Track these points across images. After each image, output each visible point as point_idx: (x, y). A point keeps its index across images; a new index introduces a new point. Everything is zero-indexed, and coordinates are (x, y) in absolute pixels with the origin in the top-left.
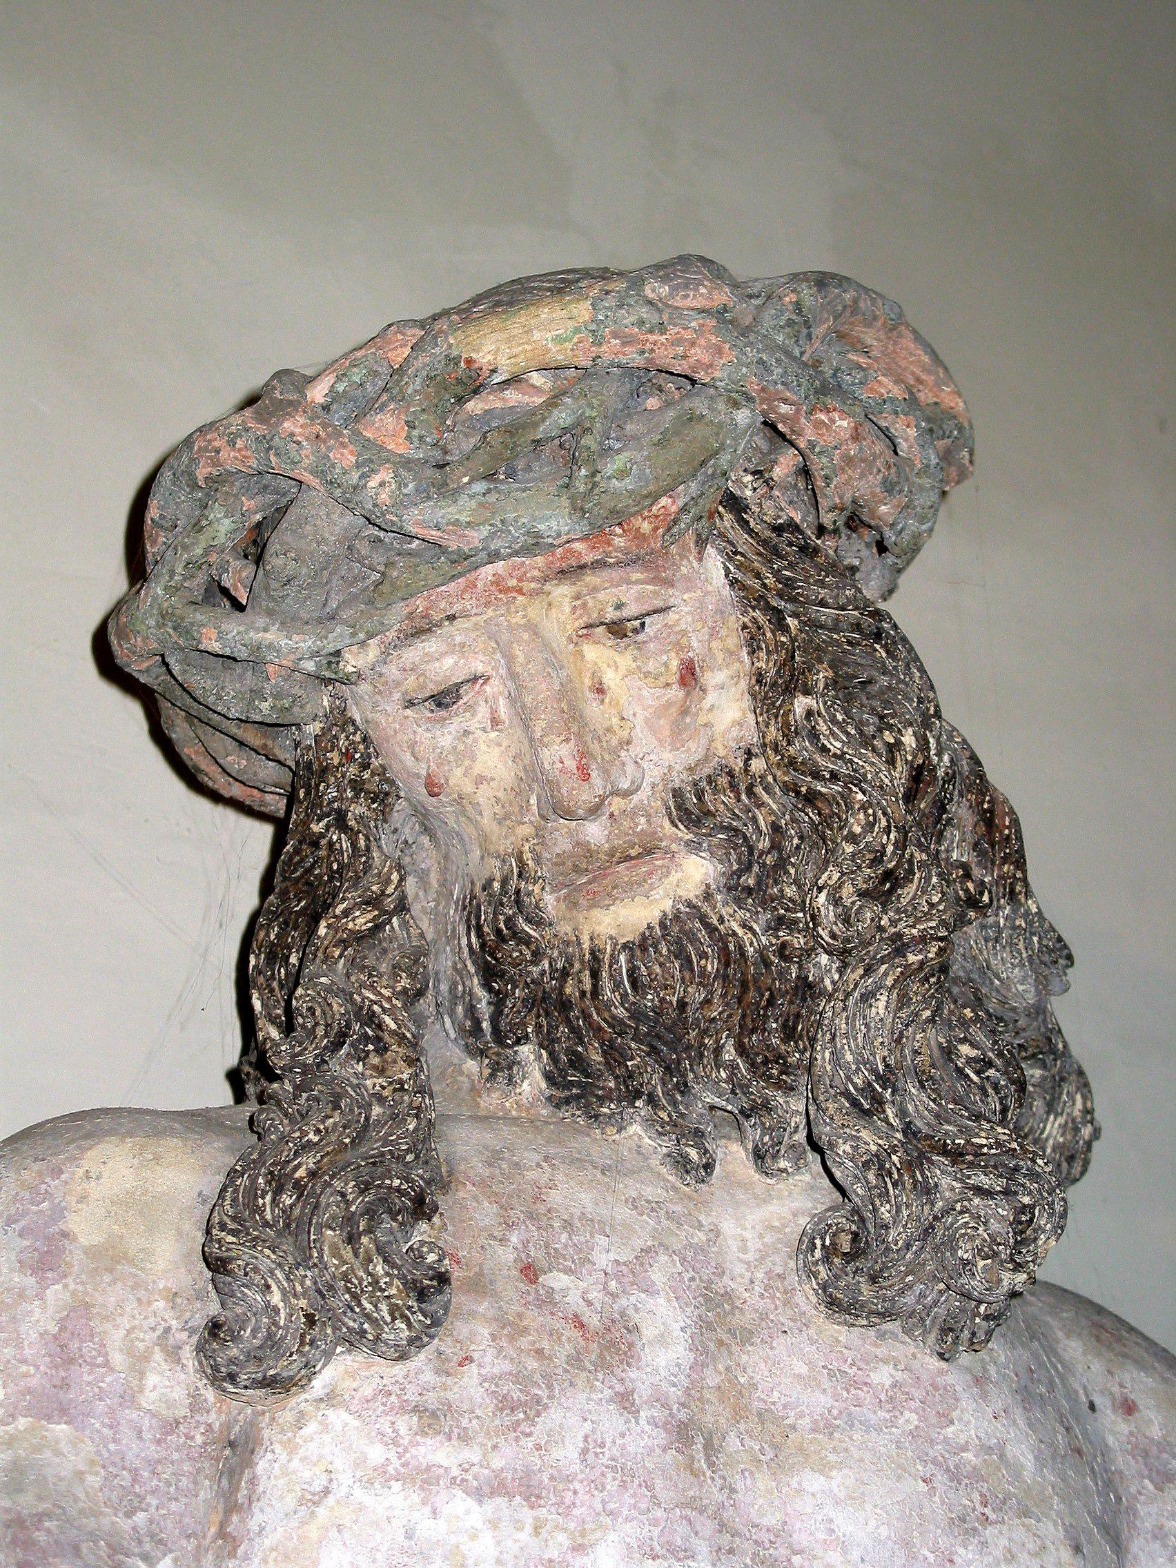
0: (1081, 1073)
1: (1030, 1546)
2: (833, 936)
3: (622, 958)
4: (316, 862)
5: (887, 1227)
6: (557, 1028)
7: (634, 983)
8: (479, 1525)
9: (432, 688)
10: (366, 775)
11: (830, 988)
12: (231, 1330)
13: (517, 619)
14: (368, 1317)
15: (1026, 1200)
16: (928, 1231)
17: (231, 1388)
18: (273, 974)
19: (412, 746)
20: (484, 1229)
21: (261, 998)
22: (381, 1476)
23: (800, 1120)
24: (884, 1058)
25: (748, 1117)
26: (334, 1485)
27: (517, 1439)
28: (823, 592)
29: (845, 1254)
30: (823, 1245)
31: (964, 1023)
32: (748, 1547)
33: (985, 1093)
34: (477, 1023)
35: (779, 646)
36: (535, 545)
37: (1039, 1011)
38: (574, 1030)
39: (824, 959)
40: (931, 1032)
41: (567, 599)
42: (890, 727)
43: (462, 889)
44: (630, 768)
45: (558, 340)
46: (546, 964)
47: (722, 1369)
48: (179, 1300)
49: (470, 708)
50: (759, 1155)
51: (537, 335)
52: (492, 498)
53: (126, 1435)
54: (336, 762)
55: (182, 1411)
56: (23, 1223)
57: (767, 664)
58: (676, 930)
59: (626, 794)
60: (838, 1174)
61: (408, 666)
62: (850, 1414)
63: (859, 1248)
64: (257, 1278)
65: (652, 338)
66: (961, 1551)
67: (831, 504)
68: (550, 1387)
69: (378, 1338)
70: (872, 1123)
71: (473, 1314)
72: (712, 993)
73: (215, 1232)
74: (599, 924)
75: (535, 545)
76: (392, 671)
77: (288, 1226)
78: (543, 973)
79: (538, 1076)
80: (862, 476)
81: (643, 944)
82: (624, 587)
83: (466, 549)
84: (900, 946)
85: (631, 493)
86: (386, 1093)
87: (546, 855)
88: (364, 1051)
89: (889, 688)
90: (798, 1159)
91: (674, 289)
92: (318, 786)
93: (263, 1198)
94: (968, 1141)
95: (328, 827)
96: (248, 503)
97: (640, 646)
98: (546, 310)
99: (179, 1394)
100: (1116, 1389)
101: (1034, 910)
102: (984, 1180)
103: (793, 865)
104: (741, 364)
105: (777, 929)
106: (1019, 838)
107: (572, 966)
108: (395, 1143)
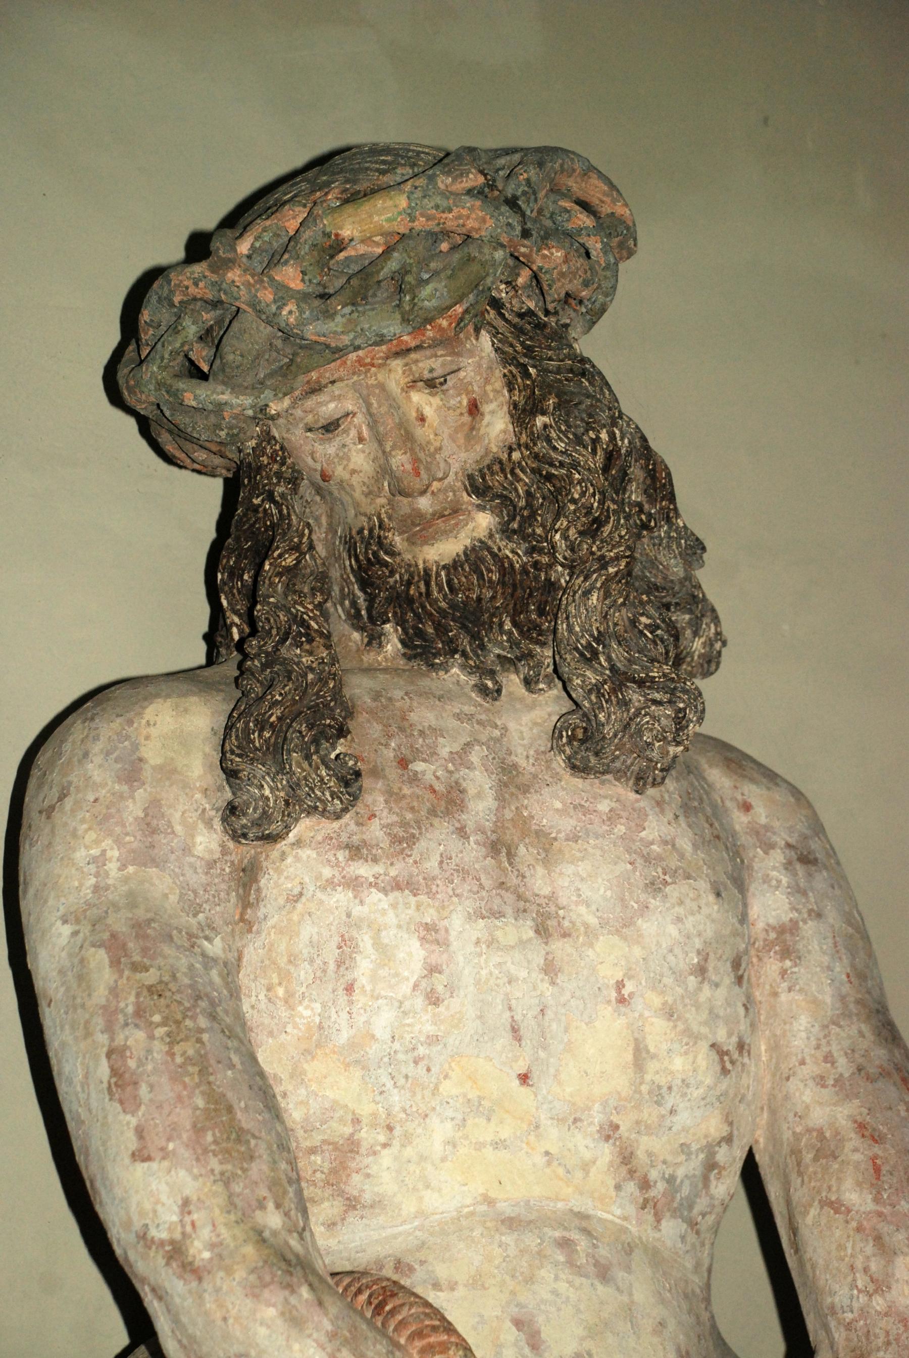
0: (713, 610)
1: (691, 895)
2: (565, 558)
3: (443, 573)
8: (386, 907)
9: (322, 422)
10: (284, 469)
11: (564, 584)
12: (242, 810)
13: (372, 381)
14: (319, 799)
15: (681, 705)
16: (627, 726)
17: (244, 841)
19: (312, 454)
20: (375, 740)
21: (227, 598)
22: (330, 885)
23: (549, 661)
25: (520, 661)
26: (305, 891)
31: (641, 603)
32: (534, 908)
33: (656, 644)
34: (358, 611)
35: (526, 387)
36: (381, 340)
37: (688, 578)
38: (417, 616)
39: (560, 568)
40: (624, 611)
42: (593, 429)
43: (344, 530)
44: (442, 465)
45: (389, 220)
46: (397, 576)
49: (346, 431)
50: (528, 683)
51: (376, 218)
52: (355, 315)
53: (189, 872)
55: (217, 855)
56: (115, 755)
59: (440, 480)
60: (574, 695)
64: (256, 782)
65: (444, 216)
66: (653, 901)
68: (420, 828)
69: (324, 810)
70: (592, 667)
71: (373, 789)
73: (228, 755)
75: (381, 340)
76: (298, 412)
77: (268, 749)
78: (396, 582)
79: (396, 640)
80: (570, 281)
81: (454, 566)
84: (604, 563)
85: (435, 308)
86: (314, 665)
87: (395, 515)
89: (592, 405)
90: (550, 684)
91: (455, 179)
94: (647, 675)
95: (263, 501)
96: (205, 316)
97: (444, 392)
99: (215, 846)
100: (739, 797)
101: (681, 524)
102: (657, 696)
104: (497, 226)
106: (671, 485)
108: (324, 697)
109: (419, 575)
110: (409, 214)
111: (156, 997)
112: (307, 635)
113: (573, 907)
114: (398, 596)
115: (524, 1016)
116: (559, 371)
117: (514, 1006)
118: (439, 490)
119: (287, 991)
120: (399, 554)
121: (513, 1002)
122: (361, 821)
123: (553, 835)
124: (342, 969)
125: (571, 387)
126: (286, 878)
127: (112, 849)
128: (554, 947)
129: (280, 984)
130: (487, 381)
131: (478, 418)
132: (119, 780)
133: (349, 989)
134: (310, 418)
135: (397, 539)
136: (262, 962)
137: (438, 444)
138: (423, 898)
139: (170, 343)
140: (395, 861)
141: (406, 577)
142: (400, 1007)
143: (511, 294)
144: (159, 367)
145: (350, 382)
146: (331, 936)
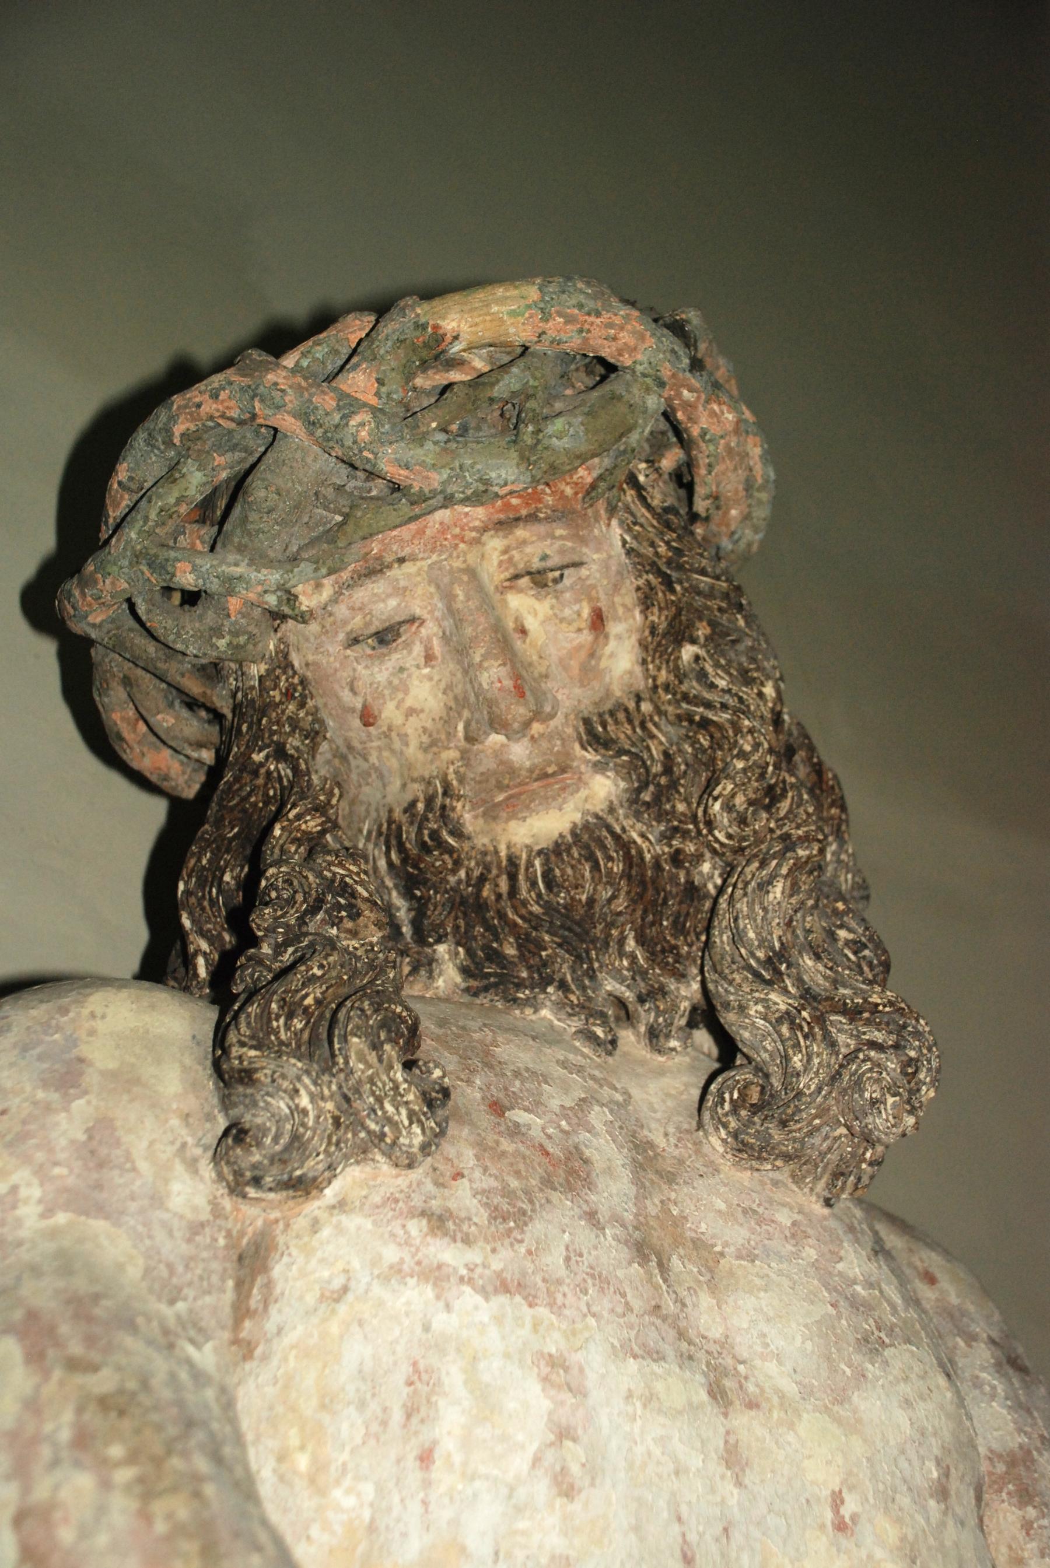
3: (537, 863)
4: (252, 791)
5: (798, 1075)
7: (550, 883)
9: (376, 626)
10: (302, 714)
14: (389, 1120)
15: (912, 1054)
16: (835, 1077)
18: (204, 896)
21: (191, 915)
22: (397, 1271)
26: (353, 1284)
27: (512, 1245)
28: (704, 562)
29: (752, 1105)
30: (731, 1099)
31: (836, 912)
38: (489, 928)
46: (462, 874)
47: (657, 1202)
48: (191, 1120)
49: (408, 645)
50: (654, 1035)
53: (160, 1235)
54: (277, 699)
55: (205, 1215)
58: (586, 837)
61: (358, 605)
62: (764, 1246)
65: (592, 319)
66: (870, 1366)
68: (531, 1202)
72: (619, 890)
76: (341, 610)
77: (299, 1047)
78: (459, 882)
81: (557, 850)
82: (549, 542)
83: (426, 491)
86: (359, 953)
92: (260, 721)
93: (277, 1020)
94: (865, 1000)
95: (267, 757)
96: (219, 460)
99: (201, 1201)
102: (879, 1036)
105: (671, 838)
107: (489, 871)
109: (499, 867)
111: (113, 1414)
112: (350, 906)
113: (758, 1362)
114: (463, 901)
115: (701, 1535)
116: (710, 595)
117: (685, 1515)
118: (542, 735)
119: (315, 1460)
120: (469, 838)
121: (684, 1509)
122: (441, 1180)
123: (718, 1249)
124: (415, 1420)
125: (724, 619)
126: (322, 1261)
127: (29, 1185)
128: (736, 1423)
129: (302, 1448)
130: (616, 588)
131: (601, 638)
132: (45, 1084)
133: (426, 1458)
134: (357, 622)
135: (467, 816)
136: (271, 1408)
137: (543, 670)
138: (543, 1311)
139: (160, 497)
140: (498, 1245)
141: (477, 873)
142: (510, 1496)
144: (139, 533)
145: (425, 564)
146: (395, 1363)
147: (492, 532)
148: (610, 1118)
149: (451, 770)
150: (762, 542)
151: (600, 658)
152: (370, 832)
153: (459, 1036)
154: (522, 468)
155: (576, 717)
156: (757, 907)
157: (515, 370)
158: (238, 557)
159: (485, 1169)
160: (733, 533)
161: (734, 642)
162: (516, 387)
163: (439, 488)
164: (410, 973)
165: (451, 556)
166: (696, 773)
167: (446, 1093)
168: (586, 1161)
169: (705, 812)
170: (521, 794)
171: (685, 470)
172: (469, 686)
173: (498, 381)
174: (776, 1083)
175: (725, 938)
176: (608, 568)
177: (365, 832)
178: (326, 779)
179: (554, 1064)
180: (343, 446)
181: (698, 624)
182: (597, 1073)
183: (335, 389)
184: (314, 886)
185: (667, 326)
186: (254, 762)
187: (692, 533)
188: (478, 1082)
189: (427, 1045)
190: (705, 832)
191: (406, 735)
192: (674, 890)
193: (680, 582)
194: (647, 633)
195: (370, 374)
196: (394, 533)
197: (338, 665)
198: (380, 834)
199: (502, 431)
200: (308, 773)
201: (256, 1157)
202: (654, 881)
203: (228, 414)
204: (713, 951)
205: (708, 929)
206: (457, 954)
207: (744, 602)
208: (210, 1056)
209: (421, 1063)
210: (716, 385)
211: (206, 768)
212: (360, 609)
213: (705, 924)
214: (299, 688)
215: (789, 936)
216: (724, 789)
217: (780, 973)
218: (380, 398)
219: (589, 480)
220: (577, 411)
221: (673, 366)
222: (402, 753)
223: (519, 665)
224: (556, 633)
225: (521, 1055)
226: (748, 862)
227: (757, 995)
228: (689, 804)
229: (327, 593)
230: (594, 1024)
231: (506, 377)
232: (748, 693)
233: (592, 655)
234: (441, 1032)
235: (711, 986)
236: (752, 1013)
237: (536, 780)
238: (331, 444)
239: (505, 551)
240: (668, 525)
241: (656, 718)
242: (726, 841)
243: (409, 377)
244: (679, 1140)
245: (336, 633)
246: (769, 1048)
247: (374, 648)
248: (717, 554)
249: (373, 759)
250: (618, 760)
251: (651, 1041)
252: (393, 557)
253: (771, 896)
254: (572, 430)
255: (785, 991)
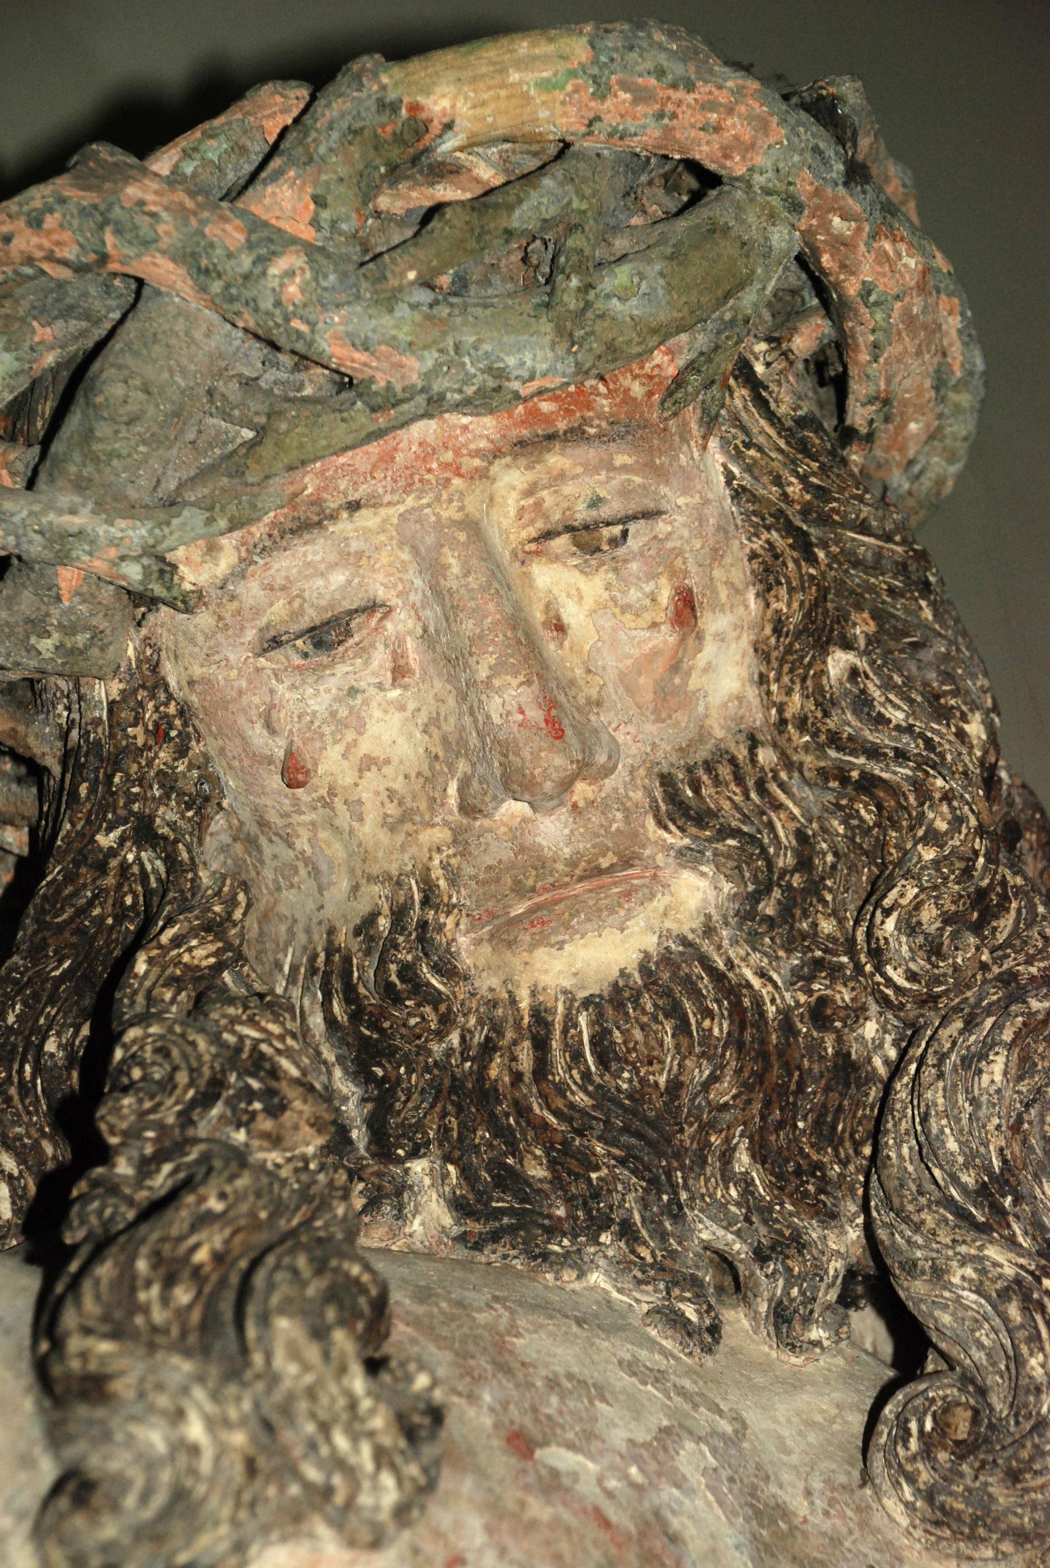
2: (912, 977)
3: (583, 1020)
4: (95, 897)
6: (474, 1131)
7: (604, 1054)
9: (311, 617)
14: (339, 1463)
18: (9, 1077)
24: (1001, 1150)
28: (866, 511)
29: (957, 1443)
30: (921, 1431)
38: (500, 1131)
41: (514, 495)
46: (455, 1038)
49: (364, 650)
54: (140, 741)
57: (789, 606)
58: (665, 976)
61: (279, 581)
63: (978, 1434)
65: (679, 94)
67: (872, 390)
72: (722, 1067)
74: (546, 972)
76: (251, 591)
77: (184, 1334)
78: (449, 1052)
83: (398, 388)
86: (284, 1173)
87: (469, 870)
88: (246, 1111)
92: (110, 778)
95: (122, 841)
96: (43, 333)
98: (525, 44)
103: (830, 890)
105: (811, 979)
107: (501, 1034)
109: (518, 1025)
110: (595, 79)
112: (269, 1094)
114: (456, 1086)
116: (876, 567)
125: (898, 608)
130: (716, 554)
131: (691, 641)
134: (278, 610)
137: (594, 693)
141: (478, 1038)
143: (777, 366)
147: (508, 459)
148: (712, 1462)
149: (437, 862)
150: (960, 478)
151: (688, 674)
152: (294, 968)
153: (453, 1318)
154: (561, 350)
155: (649, 774)
156: (961, 1098)
157: (547, 182)
158: (77, 499)
159: (503, 1552)
160: (911, 463)
161: (914, 646)
162: (551, 211)
163: (420, 384)
164: (365, 1210)
165: (438, 498)
166: (852, 868)
167: (436, 1415)
168: (674, 1539)
169: (869, 934)
170: (556, 902)
171: (832, 353)
172: (467, 720)
173: (520, 201)
174: (999, 1404)
175: (905, 1150)
176: (701, 520)
177: (286, 969)
178: (224, 877)
179: (616, 1368)
180: (256, 310)
181: (854, 616)
182: (687, 1383)
183: (244, 214)
184: (207, 1058)
185: (806, 107)
186: (100, 849)
187: (844, 462)
188: (487, 1398)
189: (400, 1331)
190: (868, 968)
191: (360, 802)
192: (816, 1068)
193: (825, 545)
194: (768, 631)
195: (301, 189)
196: (342, 460)
197: (244, 684)
198: (313, 971)
199: (526, 287)
200: (193, 866)
201: (110, 1530)
202: (782, 1052)
203: (59, 254)
204: (885, 1173)
205: (876, 1135)
206: (445, 1176)
207: (932, 579)
208: (27, 1355)
209: (393, 1364)
210: (890, 209)
211: (11, 860)
212: (283, 588)
213: (871, 1126)
214: (178, 722)
215: (1017, 1149)
216: (902, 895)
217: (1002, 1212)
218: (319, 228)
219: (671, 371)
220: (653, 254)
221: (817, 176)
222: (351, 832)
223: (553, 684)
224: (614, 630)
225: (559, 1351)
226: (945, 1021)
227: (963, 1249)
228: (841, 921)
229: (226, 561)
230: (683, 1299)
231: (534, 194)
232: (940, 732)
233: (675, 667)
234: (420, 1310)
235: (882, 1234)
236: (956, 1280)
237: (581, 879)
238: (237, 306)
239: (529, 492)
240: (804, 448)
241: (783, 775)
242: (907, 985)
243: (368, 195)
244: (831, 1502)
245: (242, 629)
246: (986, 1342)
247: (306, 655)
248: (883, 498)
249: (302, 843)
250: (719, 846)
251: (777, 1328)
252: (341, 500)
253: (985, 1078)
254: (644, 285)
255: (1011, 1242)
